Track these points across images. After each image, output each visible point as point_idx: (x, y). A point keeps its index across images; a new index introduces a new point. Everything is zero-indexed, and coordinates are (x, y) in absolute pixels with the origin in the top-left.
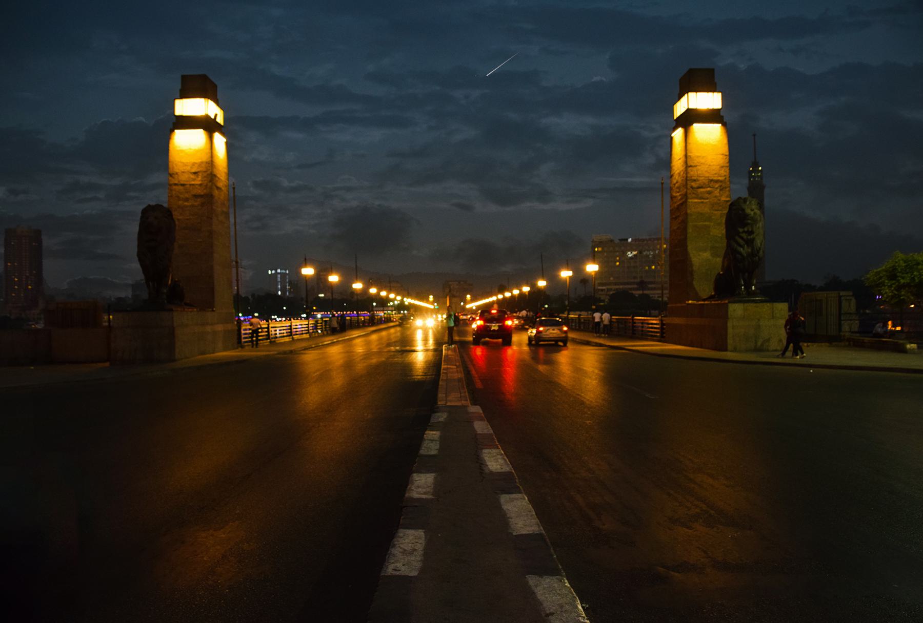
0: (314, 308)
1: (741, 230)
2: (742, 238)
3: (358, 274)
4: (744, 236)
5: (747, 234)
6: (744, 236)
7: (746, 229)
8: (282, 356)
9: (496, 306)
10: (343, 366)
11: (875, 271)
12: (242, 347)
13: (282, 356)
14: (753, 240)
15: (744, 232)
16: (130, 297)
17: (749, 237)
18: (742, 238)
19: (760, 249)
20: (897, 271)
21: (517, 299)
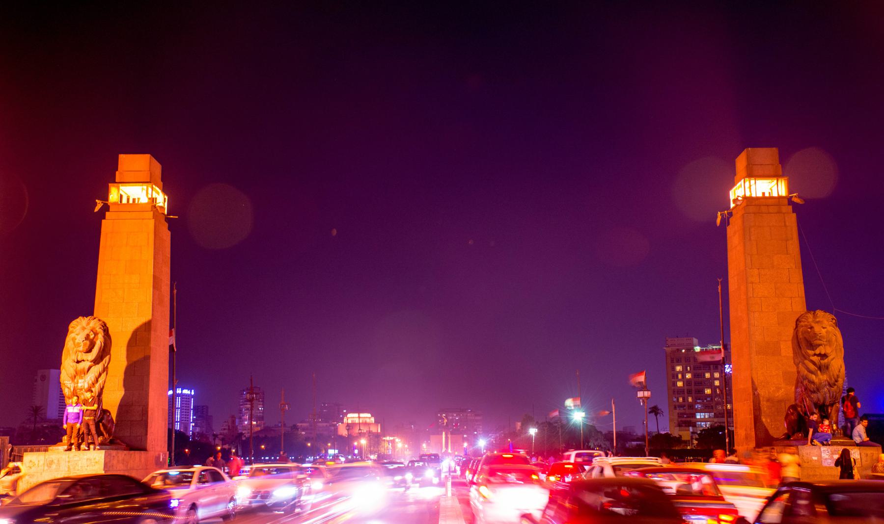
0: (345, 411)
1: (811, 352)
2: (814, 363)
3: (398, 461)
4: (815, 359)
5: (819, 358)
6: (815, 359)
7: (817, 352)
8: (173, 454)
9: (208, 461)
10: (107, 457)
11: (220, 458)
12: (816, 405)
13: (173, 454)
14: (827, 367)
15: (815, 355)
16: (734, 448)
17: (822, 361)
18: (814, 363)
19: (838, 376)
20: (240, 453)
21: (588, 416)
